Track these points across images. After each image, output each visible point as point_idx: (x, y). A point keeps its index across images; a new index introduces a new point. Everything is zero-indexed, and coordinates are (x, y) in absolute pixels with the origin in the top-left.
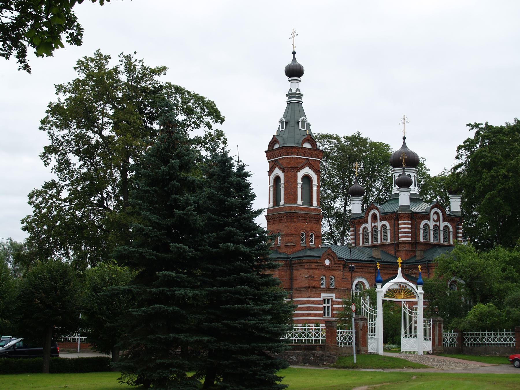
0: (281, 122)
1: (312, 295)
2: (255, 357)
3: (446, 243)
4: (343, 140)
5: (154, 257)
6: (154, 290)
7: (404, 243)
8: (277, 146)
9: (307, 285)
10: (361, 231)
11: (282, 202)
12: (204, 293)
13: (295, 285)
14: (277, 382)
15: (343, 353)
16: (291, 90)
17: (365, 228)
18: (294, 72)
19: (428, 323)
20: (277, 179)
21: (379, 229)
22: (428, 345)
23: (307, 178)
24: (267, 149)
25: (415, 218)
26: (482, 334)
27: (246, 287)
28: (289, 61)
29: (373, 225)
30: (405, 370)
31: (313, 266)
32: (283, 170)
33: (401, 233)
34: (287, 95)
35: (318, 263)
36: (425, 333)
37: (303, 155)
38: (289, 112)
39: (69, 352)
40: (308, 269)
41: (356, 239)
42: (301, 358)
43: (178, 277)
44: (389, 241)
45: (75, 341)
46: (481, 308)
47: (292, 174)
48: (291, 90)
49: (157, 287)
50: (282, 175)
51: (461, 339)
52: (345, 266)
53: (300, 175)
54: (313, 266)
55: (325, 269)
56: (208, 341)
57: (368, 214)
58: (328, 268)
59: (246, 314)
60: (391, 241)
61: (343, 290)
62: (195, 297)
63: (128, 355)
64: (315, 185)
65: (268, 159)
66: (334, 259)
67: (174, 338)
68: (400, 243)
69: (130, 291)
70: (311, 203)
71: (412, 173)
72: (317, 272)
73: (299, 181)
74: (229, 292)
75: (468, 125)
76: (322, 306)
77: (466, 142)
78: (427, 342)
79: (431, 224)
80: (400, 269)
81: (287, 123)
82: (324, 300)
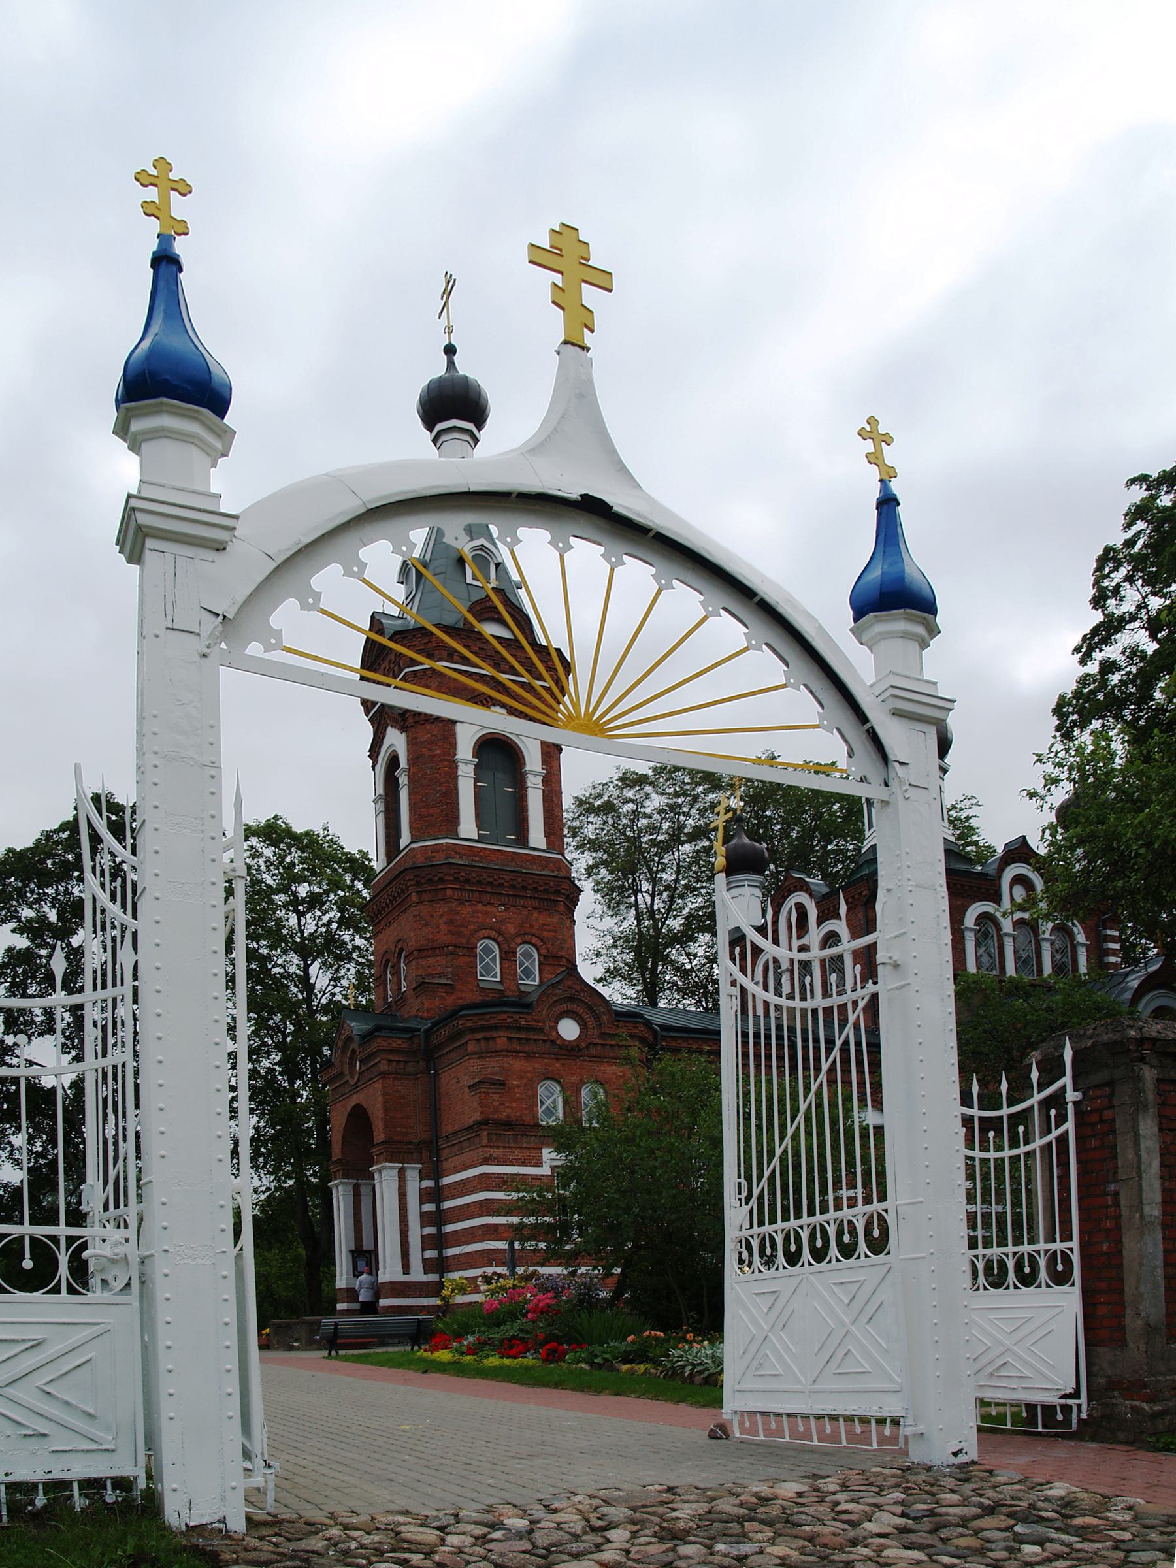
1: (496, 1152)
9: (477, 1116)
11: (405, 839)
13: (447, 1128)
19: (1020, 1090)
22: (1040, 1339)
31: (502, 1043)
35: (520, 1029)
36: (997, 1212)
38: (486, 616)
40: (480, 1054)
54: (502, 1043)
58: (570, 1050)
64: (536, 774)
66: (597, 1017)
72: (518, 1064)
75: (1132, 481)
78: (1016, 1300)
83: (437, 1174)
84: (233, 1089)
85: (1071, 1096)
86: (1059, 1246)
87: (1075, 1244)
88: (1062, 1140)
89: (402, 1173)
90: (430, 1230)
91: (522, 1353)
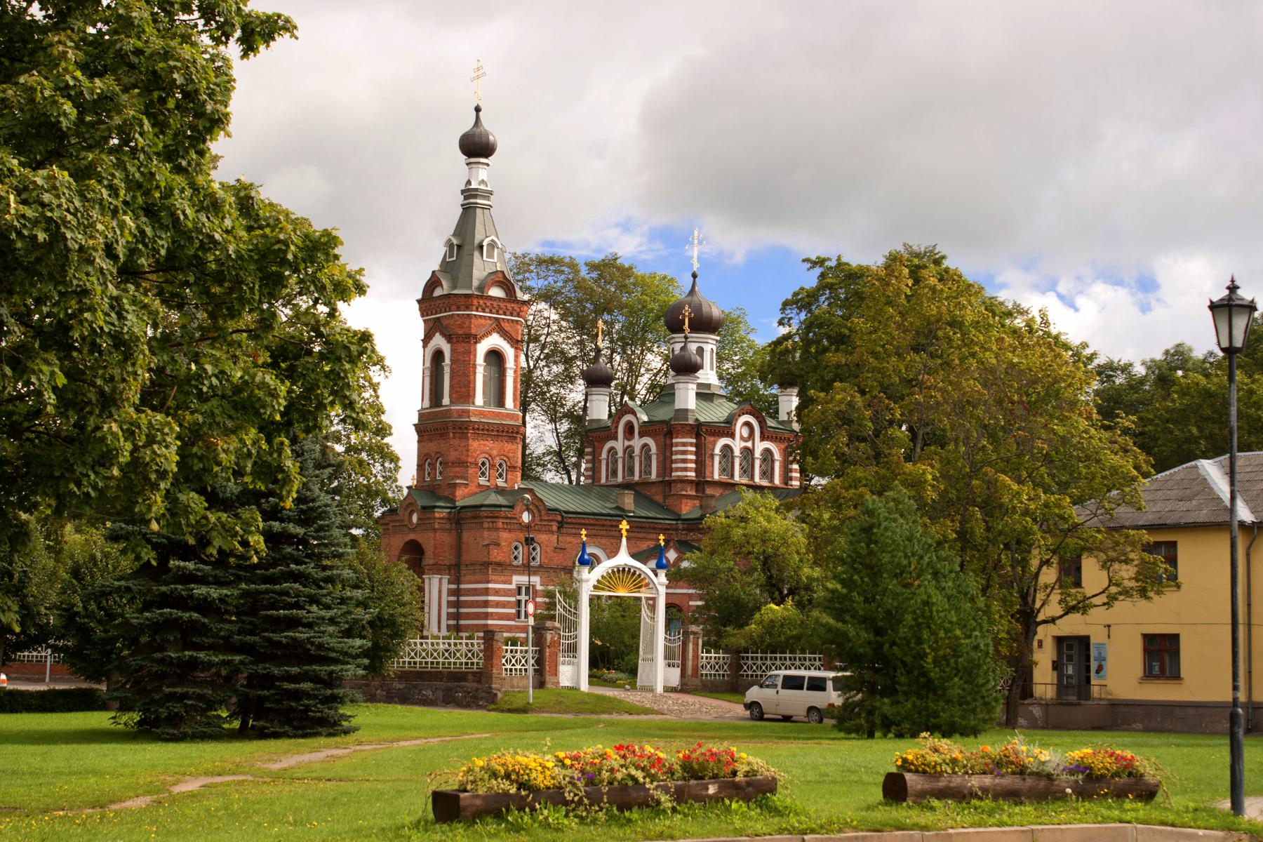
0: (450, 245)
2: (306, 686)
3: (765, 483)
4: (584, 272)
5: (164, 541)
6: (163, 588)
8: (438, 292)
10: (604, 455)
11: (446, 400)
12: (236, 592)
13: (466, 558)
14: (344, 723)
15: (513, 687)
16: (469, 182)
17: (612, 449)
18: (476, 147)
20: (438, 356)
21: (637, 451)
23: (495, 357)
24: (420, 296)
25: (703, 432)
27: (297, 585)
28: (467, 125)
29: (627, 443)
30: (615, 717)
31: (500, 525)
32: (449, 338)
33: (677, 461)
34: (463, 192)
36: (669, 655)
39: (29, 680)
40: (489, 529)
41: (595, 470)
42: (441, 694)
43: (198, 570)
44: (654, 476)
45: (41, 662)
46: (773, 610)
47: (466, 346)
48: (469, 182)
49: (167, 583)
50: (446, 349)
51: (736, 667)
52: (561, 525)
53: (482, 348)
56: (242, 662)
57: (618, 423)
59: (294, 623)
60: (658, 476)
61: (556, 570)
62: (222, 600)
63: (125, 684)
65: (422, 315)
66: (539, 511)
67: (191, 656)
68: (674, 481)
69: (128, 589)
70: (501, 403)
71: (710, 344)
74: (273, 592)
76: (513, 599)
77: (796, 294)
78: (672, 669)
79: (737, 445)
80: (624, 540)
81: (459, 247)
82: (519, 589)
83: (458, 582)
84: (895, 788)
89: (440, 580)
90: (452, 610)
91: (171, 693)
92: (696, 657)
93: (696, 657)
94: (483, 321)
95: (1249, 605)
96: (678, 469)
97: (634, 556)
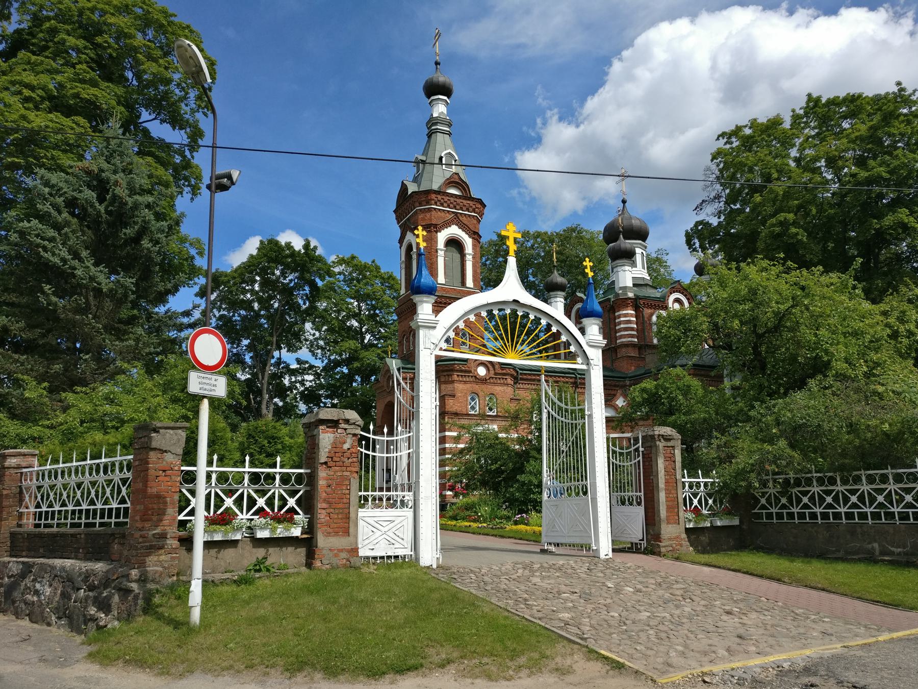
7: (626, 345)
26: (255, 478)
33: (620, 330)
37: (445, 205)
53: (442, 237)
55: (477, 383)
58: (483, 381)
64: (469, 254)
70: (463, 283)
73: (441, 244)
75: (718, 139)
78: (627, 509)
80: (512, 261)
85: (641, 449)
86: (638, 494)
87: (642, 494)
88: (639, 462)
92: (672, 483)
93: (672, 483)
94: (443, 214)
95: (497, 550)
96: (621, 337)
97: (529, 286)
